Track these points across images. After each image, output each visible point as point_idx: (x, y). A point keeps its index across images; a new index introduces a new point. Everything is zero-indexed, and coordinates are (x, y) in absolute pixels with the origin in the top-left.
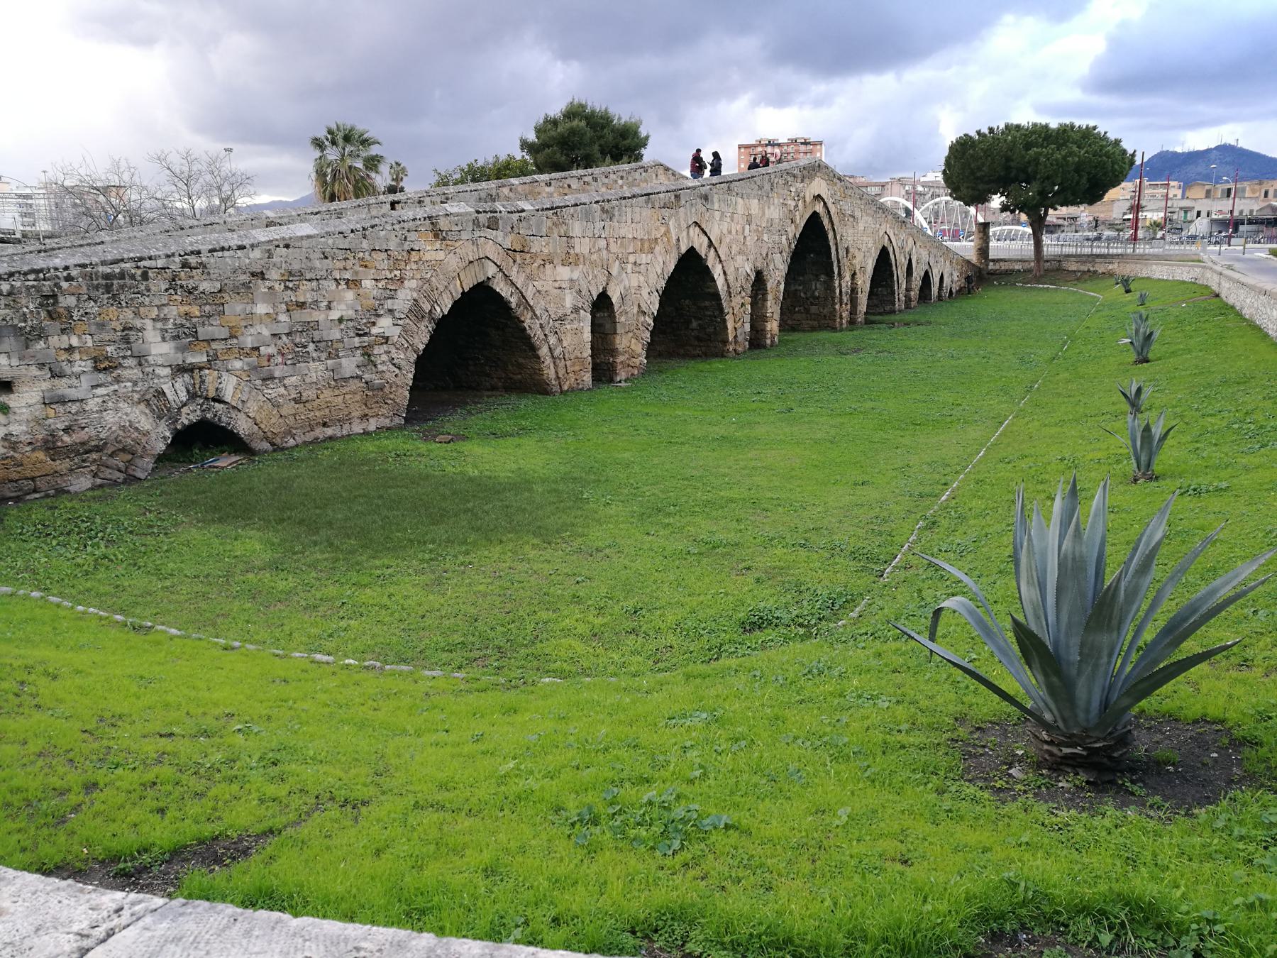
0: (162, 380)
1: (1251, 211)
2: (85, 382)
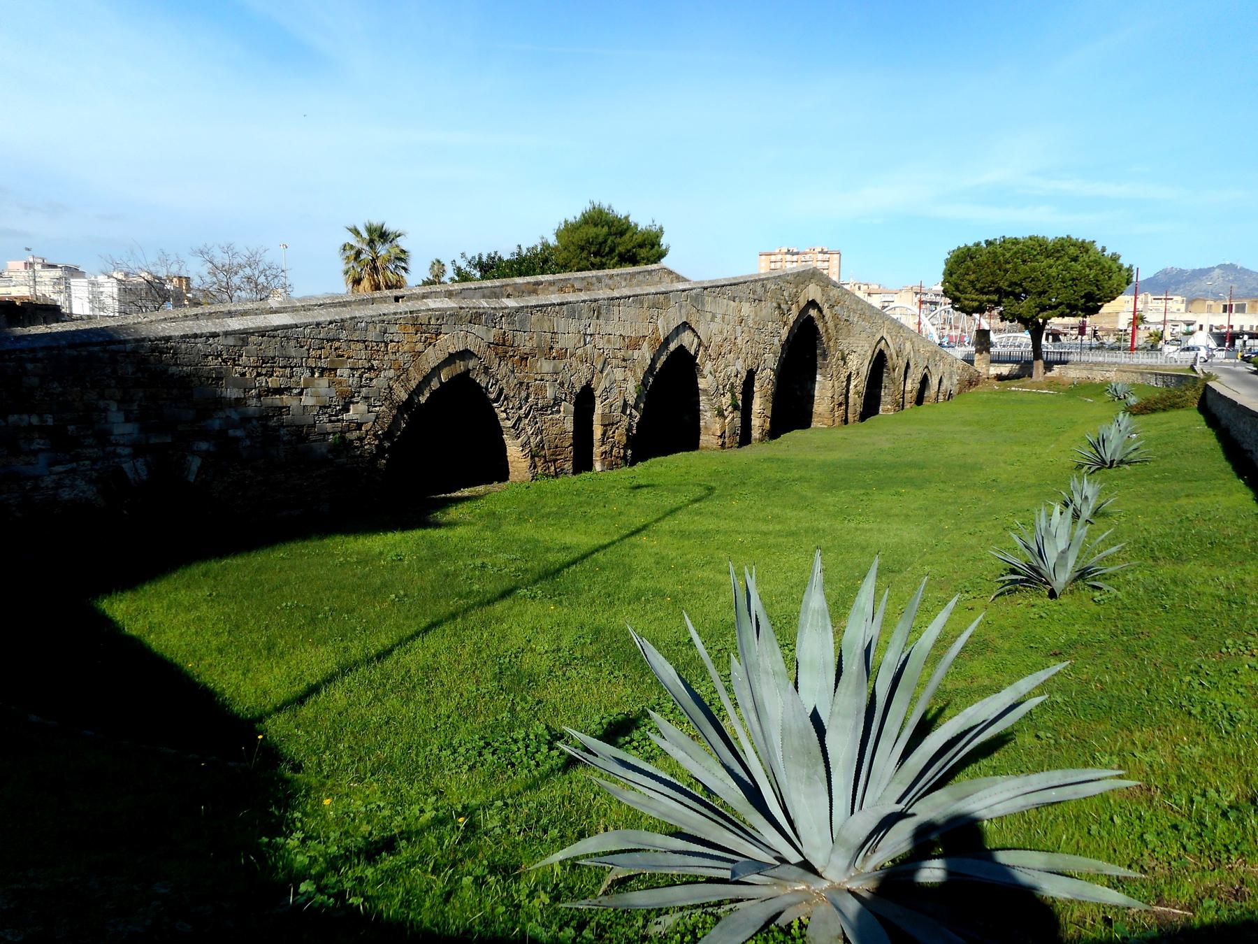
0: (123, 459)
1: (1252, 327)
2: (42, 459)
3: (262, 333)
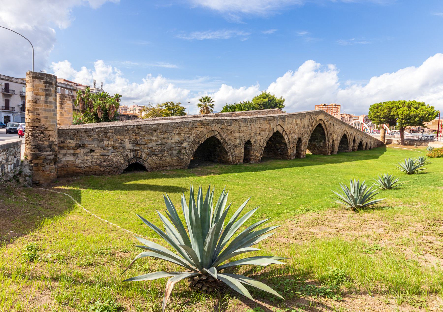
2: (110, 152)
3: (163, 124)
